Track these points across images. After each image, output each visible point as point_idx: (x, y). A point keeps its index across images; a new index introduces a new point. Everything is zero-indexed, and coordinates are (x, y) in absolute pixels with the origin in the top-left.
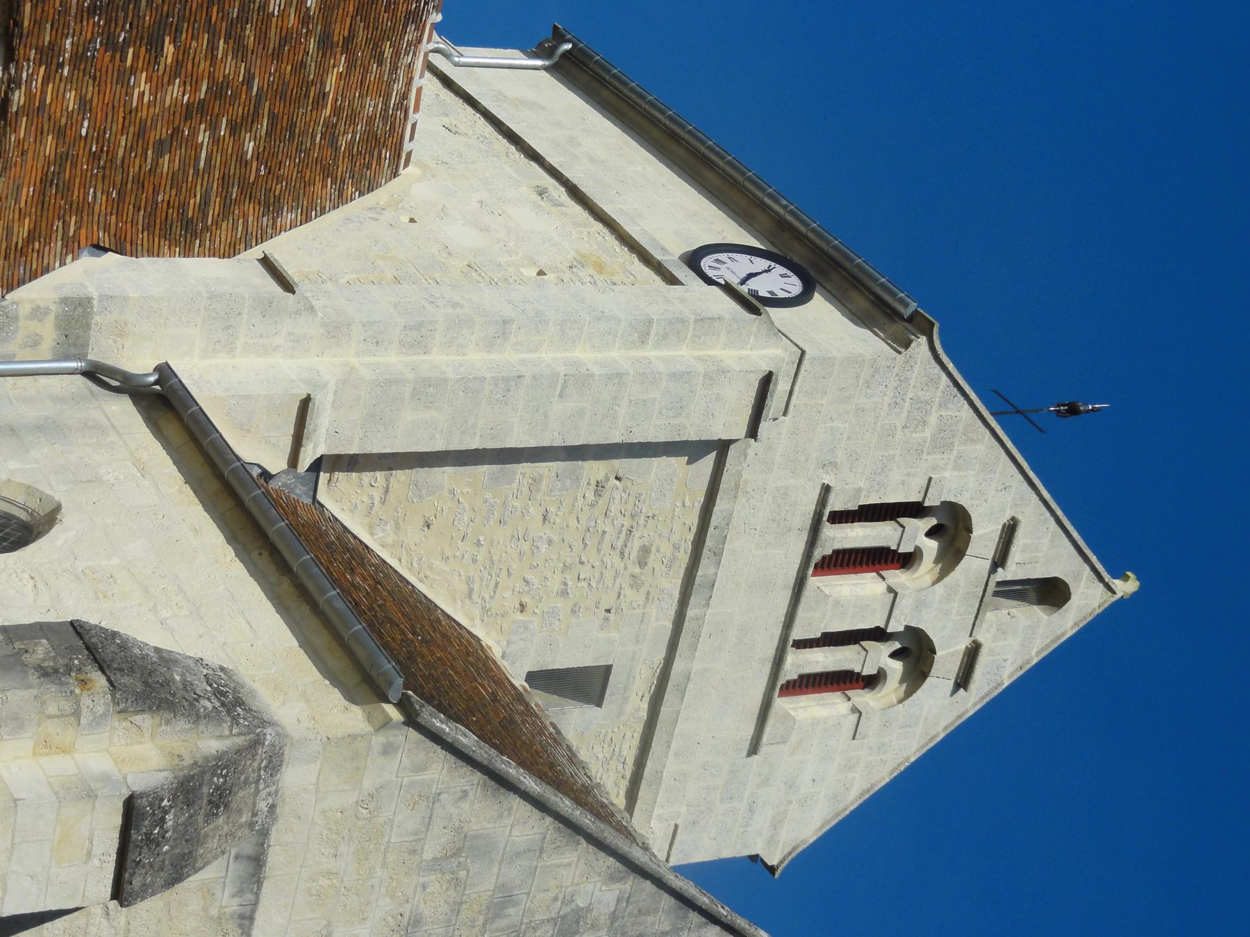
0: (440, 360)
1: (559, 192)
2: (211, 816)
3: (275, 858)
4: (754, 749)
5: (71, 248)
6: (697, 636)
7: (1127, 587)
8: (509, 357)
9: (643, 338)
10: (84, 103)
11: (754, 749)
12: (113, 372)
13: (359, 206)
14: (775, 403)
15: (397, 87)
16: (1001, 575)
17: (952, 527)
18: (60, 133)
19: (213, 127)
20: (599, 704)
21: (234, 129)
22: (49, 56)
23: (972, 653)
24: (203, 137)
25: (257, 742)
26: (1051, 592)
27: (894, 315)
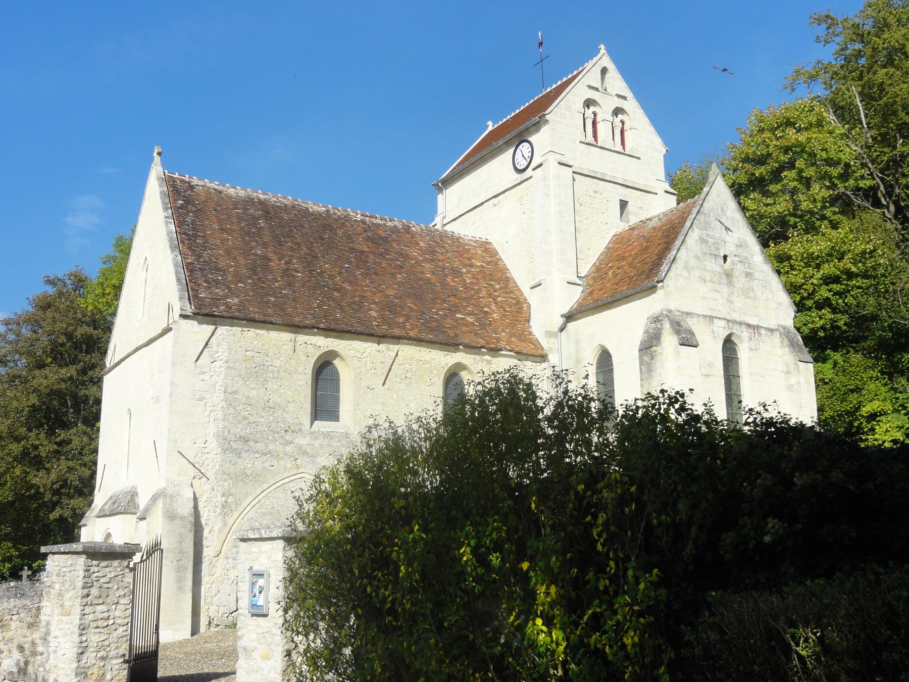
4: (639, 158)
5: (531, 333)
7: (603, 50)
11: (639, 158)
13: (502, 255)
14: (564, 161)
17: (588, 103)
21: (495, 291)
23: (619, 96)
26: (604, 71)
27: (538, 122)
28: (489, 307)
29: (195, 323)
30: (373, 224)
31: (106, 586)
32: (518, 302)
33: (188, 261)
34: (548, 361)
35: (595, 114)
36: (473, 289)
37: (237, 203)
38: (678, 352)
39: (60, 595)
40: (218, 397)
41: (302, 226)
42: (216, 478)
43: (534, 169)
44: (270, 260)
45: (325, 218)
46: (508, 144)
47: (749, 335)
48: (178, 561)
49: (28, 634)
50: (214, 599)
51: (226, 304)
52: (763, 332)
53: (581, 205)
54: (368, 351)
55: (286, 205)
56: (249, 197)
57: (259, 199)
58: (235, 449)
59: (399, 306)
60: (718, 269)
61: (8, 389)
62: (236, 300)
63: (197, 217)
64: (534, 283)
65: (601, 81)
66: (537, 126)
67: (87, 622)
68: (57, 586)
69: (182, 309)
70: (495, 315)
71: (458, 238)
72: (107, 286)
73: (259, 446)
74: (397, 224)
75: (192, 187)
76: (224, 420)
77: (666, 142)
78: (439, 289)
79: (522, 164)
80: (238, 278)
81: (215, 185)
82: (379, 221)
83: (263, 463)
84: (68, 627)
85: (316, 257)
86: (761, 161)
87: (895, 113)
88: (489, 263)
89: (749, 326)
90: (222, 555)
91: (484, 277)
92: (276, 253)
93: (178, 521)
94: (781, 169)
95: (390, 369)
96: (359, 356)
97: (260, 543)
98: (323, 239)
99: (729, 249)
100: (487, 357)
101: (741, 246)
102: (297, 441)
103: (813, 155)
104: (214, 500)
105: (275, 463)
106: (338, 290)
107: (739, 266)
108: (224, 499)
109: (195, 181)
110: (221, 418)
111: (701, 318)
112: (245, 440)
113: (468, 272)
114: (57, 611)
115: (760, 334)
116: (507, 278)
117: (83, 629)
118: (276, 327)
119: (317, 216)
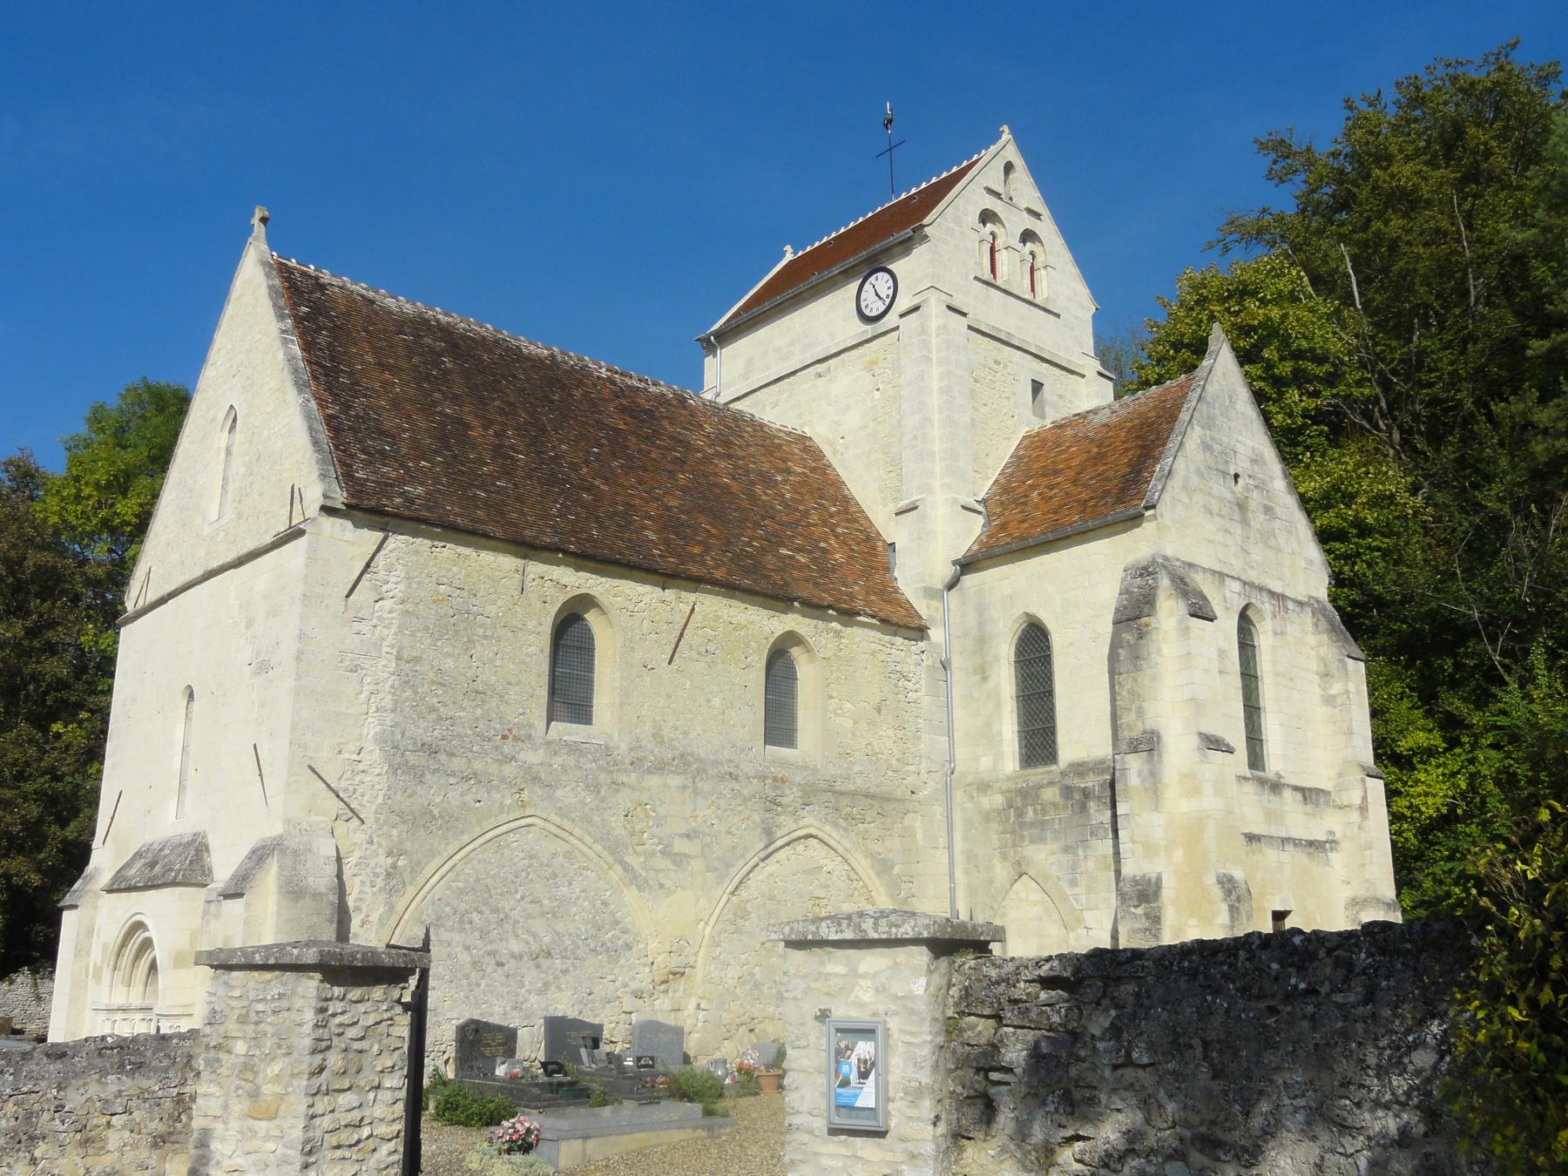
1: (820, 368)
3: (1188, 559)
4: (1058, 316)
5: (896, 590)
7: (1006, 136)
9: (930, 359)
11: (1058, 316)
14: (956, 304)
21: (831, 516)
23: (1030, 211)
26: (1009, 168)
27: (910, 238)
29: (349, 524)
30: (628, 387)
31: (357, 1046)
32: (868, 538)
33: (330, 412)
36: (797, 510)
37: (402, 323)
38: (1188, 628)
39: (248, 1068)
40: (384, 668)
41: (514, 377)
43: (901, 316)
44: (468, 426)
45: (549, 368)
46: (847, 275)
49: (153, 1162)
51: (403, 494)
52: (1290, 605)
54: (646, 600)
55: (484, 338)
56: (420, 314)
57: (438, 321)
58: (414, 767)
59: (689, 526)
60: (1229, 496)
61: (1319, 233)
62: (420, 490)
63: (336, 338)
64: (903, 504)
65: (999, 182)
66: (906, 246)
67: (318, 1133)
68: (240, 1047)
69: (325, 496)
70: (837, 556)
71: (762, 425)
72: (87, 484)
73: (457, 763)
74: (664, 390)
75: (322, 287)
76: (394, 711)
77: (1096, 294)
78: (745, 504)
79: (875, 308)
80: (420, 453)
81: (360, 288)
82: (635, 383)
83: (462, 795)
84: (271, 1146)
85: (545, 431)
87: (1410, 290)
88: (813, 470)
89: (1272, 594)
91: (811, 492)
92: (477, 416)
93: (308, 902)
97: (852, 952)
98: (552, 401)
99: (1241, 465)
103: (1286, 340)
104: (373, 862)
106: (588, 490)
107: (1255, 494)
108: (390, 861)
109: (326, 277)
110: (390, 706)
112: (431, 750)
113: (785, 481)
114: (238, 1107)
115: (1286, 608)
116: (845, 496)
117: (310, 1153)
118: (493, 543)
119: (535, 363)
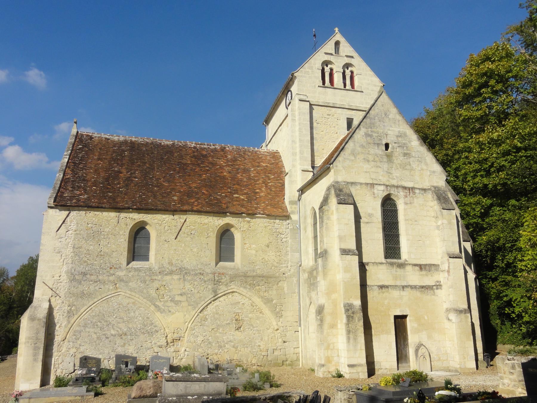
0: (298, 150)
2: (343, 191)
3: (352, 181)
4: (362, 92)
6: (342, 105)
7: (337, 30)
8: (297, 140)
10: (263, 203)
11: (362, 92)
12: (299, 198)
15: (266, 154)
16: (334, 53)
17: (326, 63)
18: (267, 206)
19: (269, 183)
20: (353, 119)
21: (269, 180)
22: (256, 208)
23: (347, 56)
24: (270, 184)
25: (334, 186)
26: (337, 44)
27: (292, 78)
28: (260, 189)
29: (58, 210)
34: (291, 219)
35: (352, 72)
40: (69, 251)
41: (153, 153)
42: (65, 296)
47: (405, 194)
48: (35, 344)
50: (60, 365)
52: (417, 191)
53: (318, 123)
54: (167, 220)
55: (147, 143)
57: (131, 141)
58: (78, 280)
73: (93, 278)
86: (470, 84)
89: (405, 188)
90: (66, 340)
93: (36, 321)
94: (480, 88)
95: (181, 229)
96: (160, 223)
100: (247, 219)
101: (400, 136)
102: (117, 273)
105: (102, 286)
108: (69, 308)
111: (364, 185)
112: (85, 274)
